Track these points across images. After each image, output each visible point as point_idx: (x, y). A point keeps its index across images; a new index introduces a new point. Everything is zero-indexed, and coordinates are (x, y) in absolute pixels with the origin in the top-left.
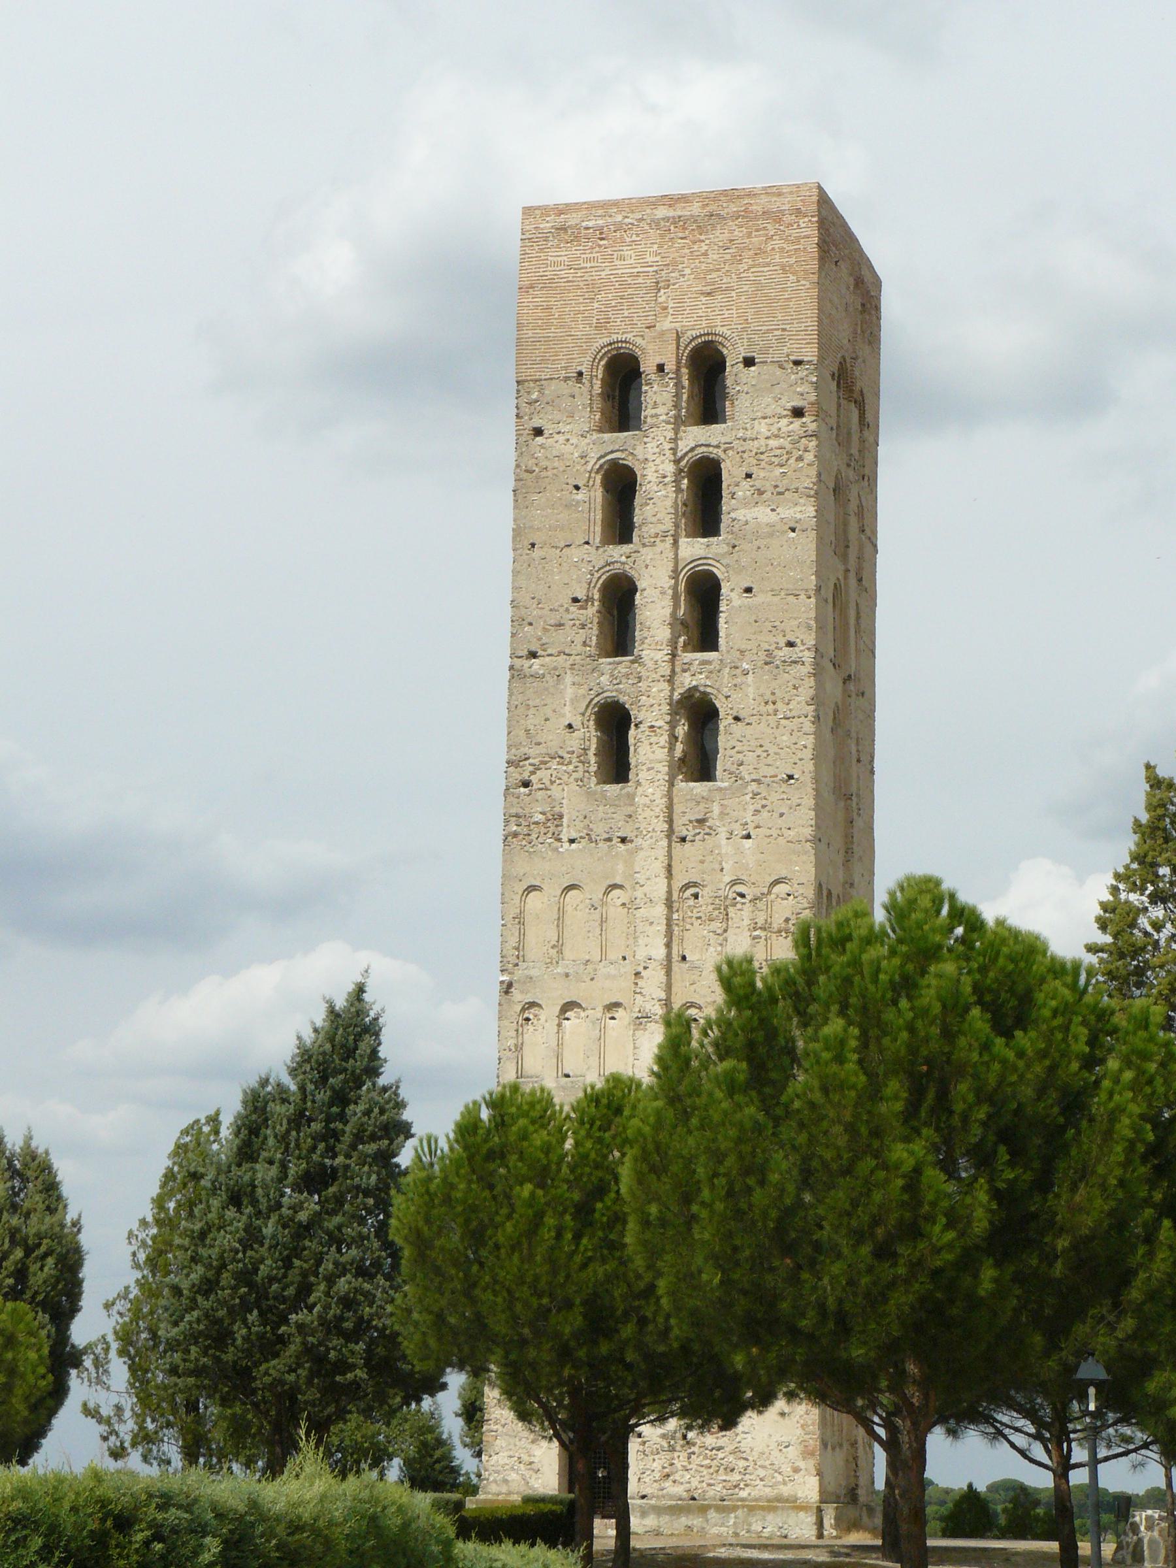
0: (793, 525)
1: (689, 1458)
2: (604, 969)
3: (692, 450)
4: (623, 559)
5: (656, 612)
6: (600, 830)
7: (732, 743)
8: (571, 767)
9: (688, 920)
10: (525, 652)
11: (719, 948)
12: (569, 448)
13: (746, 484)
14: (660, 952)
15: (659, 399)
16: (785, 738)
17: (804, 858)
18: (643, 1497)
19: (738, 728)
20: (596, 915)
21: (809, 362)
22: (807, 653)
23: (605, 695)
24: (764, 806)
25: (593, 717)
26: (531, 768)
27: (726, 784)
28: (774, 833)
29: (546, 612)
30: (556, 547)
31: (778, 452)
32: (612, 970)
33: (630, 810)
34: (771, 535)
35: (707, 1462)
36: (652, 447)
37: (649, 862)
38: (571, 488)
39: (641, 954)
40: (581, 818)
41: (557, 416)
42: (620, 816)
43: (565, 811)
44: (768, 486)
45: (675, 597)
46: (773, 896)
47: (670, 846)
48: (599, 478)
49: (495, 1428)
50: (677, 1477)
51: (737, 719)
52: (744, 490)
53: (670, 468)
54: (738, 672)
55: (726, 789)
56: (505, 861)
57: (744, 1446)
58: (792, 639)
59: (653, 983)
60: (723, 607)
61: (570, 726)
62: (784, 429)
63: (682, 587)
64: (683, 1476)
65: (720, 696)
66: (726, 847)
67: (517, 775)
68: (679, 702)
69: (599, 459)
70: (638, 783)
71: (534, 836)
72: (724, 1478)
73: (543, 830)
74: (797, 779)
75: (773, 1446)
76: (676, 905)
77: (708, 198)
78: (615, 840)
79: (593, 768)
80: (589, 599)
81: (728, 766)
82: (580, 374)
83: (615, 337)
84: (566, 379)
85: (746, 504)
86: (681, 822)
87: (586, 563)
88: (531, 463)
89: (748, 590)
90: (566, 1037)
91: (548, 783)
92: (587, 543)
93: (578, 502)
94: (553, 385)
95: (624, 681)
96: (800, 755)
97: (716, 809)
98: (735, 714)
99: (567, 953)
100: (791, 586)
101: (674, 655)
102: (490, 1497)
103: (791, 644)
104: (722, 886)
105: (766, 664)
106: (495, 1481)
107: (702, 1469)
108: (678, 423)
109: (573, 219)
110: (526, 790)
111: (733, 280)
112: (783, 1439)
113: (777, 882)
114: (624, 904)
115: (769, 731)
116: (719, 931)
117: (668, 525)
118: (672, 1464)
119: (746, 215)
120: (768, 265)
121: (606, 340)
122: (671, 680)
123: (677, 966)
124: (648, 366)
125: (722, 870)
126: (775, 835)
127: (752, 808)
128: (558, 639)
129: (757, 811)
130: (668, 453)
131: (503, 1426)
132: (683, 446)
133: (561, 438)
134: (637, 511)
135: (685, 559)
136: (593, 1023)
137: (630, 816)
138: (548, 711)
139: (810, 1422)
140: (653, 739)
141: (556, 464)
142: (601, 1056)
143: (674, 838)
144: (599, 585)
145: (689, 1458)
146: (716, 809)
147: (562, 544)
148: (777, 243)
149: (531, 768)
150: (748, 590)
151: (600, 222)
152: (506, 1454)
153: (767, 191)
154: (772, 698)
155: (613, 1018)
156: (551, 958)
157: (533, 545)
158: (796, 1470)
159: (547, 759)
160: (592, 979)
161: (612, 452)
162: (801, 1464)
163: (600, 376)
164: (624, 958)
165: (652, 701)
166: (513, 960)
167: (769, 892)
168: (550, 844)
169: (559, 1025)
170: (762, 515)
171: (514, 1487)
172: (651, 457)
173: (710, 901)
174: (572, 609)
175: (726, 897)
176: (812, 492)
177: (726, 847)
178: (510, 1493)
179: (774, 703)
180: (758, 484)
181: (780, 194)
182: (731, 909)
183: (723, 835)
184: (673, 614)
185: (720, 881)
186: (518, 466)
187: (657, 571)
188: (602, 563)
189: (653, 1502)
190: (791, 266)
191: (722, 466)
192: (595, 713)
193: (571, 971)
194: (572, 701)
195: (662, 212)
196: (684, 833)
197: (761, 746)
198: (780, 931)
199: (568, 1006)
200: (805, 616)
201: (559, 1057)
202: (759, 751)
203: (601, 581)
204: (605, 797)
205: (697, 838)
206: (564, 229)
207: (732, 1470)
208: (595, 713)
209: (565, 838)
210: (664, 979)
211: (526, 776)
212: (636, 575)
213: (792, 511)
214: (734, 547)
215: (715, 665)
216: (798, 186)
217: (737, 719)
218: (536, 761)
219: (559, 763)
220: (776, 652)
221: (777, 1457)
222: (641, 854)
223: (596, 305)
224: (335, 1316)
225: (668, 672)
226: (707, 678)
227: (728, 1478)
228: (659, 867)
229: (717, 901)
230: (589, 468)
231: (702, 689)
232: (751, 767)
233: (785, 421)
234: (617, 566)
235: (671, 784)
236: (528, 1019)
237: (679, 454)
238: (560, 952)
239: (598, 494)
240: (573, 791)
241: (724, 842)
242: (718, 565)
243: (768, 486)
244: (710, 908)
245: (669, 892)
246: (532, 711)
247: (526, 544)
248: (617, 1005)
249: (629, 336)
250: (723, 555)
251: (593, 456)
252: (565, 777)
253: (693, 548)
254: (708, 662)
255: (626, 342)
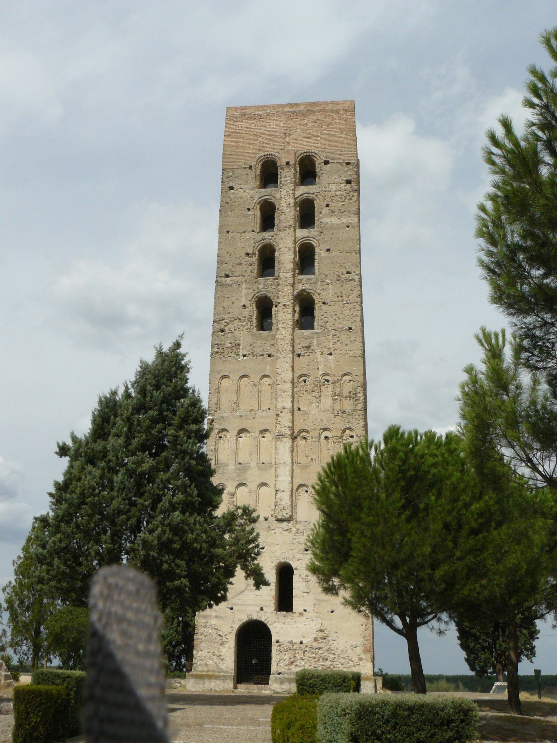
0: (348, 225)
1: (304, 653)
2: (259, 414)
3: (302, 195)
4: (270, 237)
5: (286, 258)
6: (258, 351)
7: (322, 313)
8: (244, 323)
9: (301, 392)
10: (224, 275)
11: (317, 404)
12: (245, 194)
13: (326, 209)
14: (289, 405)
15: (287, 176)
16: (347, 312)
17: (359, 364)
18: (279, 674)
19: (324, 307)
20: (256, 389)
21: (353, 163)
22: (356, 276)
23: (261, 293)
24: (338, 341)
25: (255, 303)
26: (225, 324)
27: (320, 331)
28: (343, 352)
29: (234, 258)
30: (239, 233)
31: (341, 196)
32: (264, 414)
33: (273, 342)
34: (339, 228)
35: (314, 655)
36: (284, 193)
37: (283, 367)
38: (246, 209)
39: (279, 406)
40: (249, 345)
41: (240, 182)
42: (268, 345)
43: (241, 342)
44: (336, 209)
45: (295, 252)
46: (343, 381)
47: (293, 357)
48: (258, 206)
49: (201, 637)
50: (297, 663)
51: (324, 303)
52: (325, 211)
53: (292, 201)
54: (324, 283)
55: (320, 333)
56: (211, 364)
57: (333, 647)
58: (349, 271)
59: (285, 419)
60: (316, 257)
61: (244, 306)
62: (343, 188)
63: (297, 249)
64: (300, 663)
65: (316, 294)
66: (320, 359)
67: (218, 327)
68: (296, 296)
69: (260, 198)
70: (278, 329)
71: (226, 353)
72: (322, 663)
73: (230, 351)
74: (353, 329)
75: (348, 647)
76: (296, 384)
77: (306, 105)
78: (265, 355)
79: (255, 324)
80: (254, 254)
81: (320, 323)
82: (251, 167)
83: (266, 153)
84: (245, 168)
85: (326, 216)
86: (298, 347)
87: (252, 239)
88: (228, 200)
89: (328, 250)
90: (240, 446)
91: (233, 330)
92: (253, 231)
93: (249, 215)
94: (239, 171)
95: (270, 287)
96: (354, 319)
97: (315, 342)
98: (323, 301)
99: (241, 406)
100: (348, 249)
101: (294, 277)
102: (198, 673)
103: (348, 273)
104: (319, 376)
105: (338, 280)
106: (200, 665)
107: (311, 659)
108: (295, 185)
109: (249, 111)
110: (223, 334)
111: (319, 133)
112: (353, 643)
113: (345, 375)
114: (269, 384)
115: (339, 308)
116: (317, 396)
117: (292, 222)
118: (295, 657)
119: (324, 111)
120: (334, 128)
121: (263, 154)
122: (293, 285)
123: (296, 412)
124: (281, 162)
125: (318, 369)
126: (344, 354)
127: (332, 341)
128: (239, 270)
129: (335, 343)
130: (291, 195)
131: (205, 636)
132: (298, 193)
133: (242, 190)
134: (276, 219)
135: (298, 237)
136: (254, 439)
137: (273, 345)
138: (234, 299)
139: (367, 635)
140: (285, 310)
141: (240, 200)
142: (258, 454)
143: (295, 354)
144: (258, 249)
145: (304, 653)
146: (315, 342)
147: (241, 231)
148: (337, 120)
149: (225, 324)
150: (328, 250)
151: (260, 113)
152: (206, 651)
153: (332, 103)
154: (341, 295)
155: (263, 437)
156: (233, 408)
157: (228, 232)
158: (361, 659)
159: (233, 320)
160: (254, 418)
161: (265, 196)
162: (364, 656)
163: (259, 168)
164: (269, 409)
165: (284, 294)
166: (214, 409)
167: (341, 379)
168: (234, 357)
169: (237, 440)
170: (334, 220)
171: (210, 667)
172: (283, 197)
173: (313, 382)
174: (245, 257)
175: (320, 381)
176: (356, 213)
177: (320, 359)
178: (208, 671)
179: (342, 297)
180: (332, 209)
181: (338, 104)
182: (322, 387)
183: (319, 353)
184: (294, 258)
185: (318, 374)
186: (222, 201)
187: (286, 241)
188: (260, 239)
189: (286, 676)
190: (344, 129)
191: (315, 202)
192: (256, 301)
193: (243, 414)
194: (245, 295)
195: (287, 109)
196: (300, 352)
197: (336, 315)
198: (346, 397)
199: (242, 431)
200: (355, 261)
201: (236, 454)
202: (335, 317)
203: (259, 247)
204: (261, 336)
205: (306, 354)
206: (244, 115)
207: (327, 660)
208: (256, 301)
209: (241, 354)
210: (291, 417)
211: (222, 327)
212: (276, 244)
213: (347, 219)
214: (321, 233)
215: (314, 281)
216: (346, 101)
217: (324, 303)
218: (227, 321)
219: (238, 322)
220: (342, 276)
221: (350, 653)
222: (279, 360)
223: (258, 141)
224: (168, 538)
225: (292, 282)
226: (310, 286)
227: (324, 664)
228: (288, 366)
229: (316, 383)
230: (255, 202)
231: (307, 291)
232: (332, 324)
233: (343, 185)
234: (266, 240)
235: (294, 331)
236: (221, 437)
237: (296, 196)
238: (238, 406)
239: (258, 213)
240: (245, 334)
241: (319, 356)
242: (314, 240)
243: (336, 209)
244: (313, 386)
245: (293, 378)
246: (226, 299)
247: (225, 231)
248: (266, 431)
249: (273, 153)
250: (317, 236)
251: (256, 197)
252: (241, 328)
253: (302, 233)
254: (311, 279)
255: (271, 155)
